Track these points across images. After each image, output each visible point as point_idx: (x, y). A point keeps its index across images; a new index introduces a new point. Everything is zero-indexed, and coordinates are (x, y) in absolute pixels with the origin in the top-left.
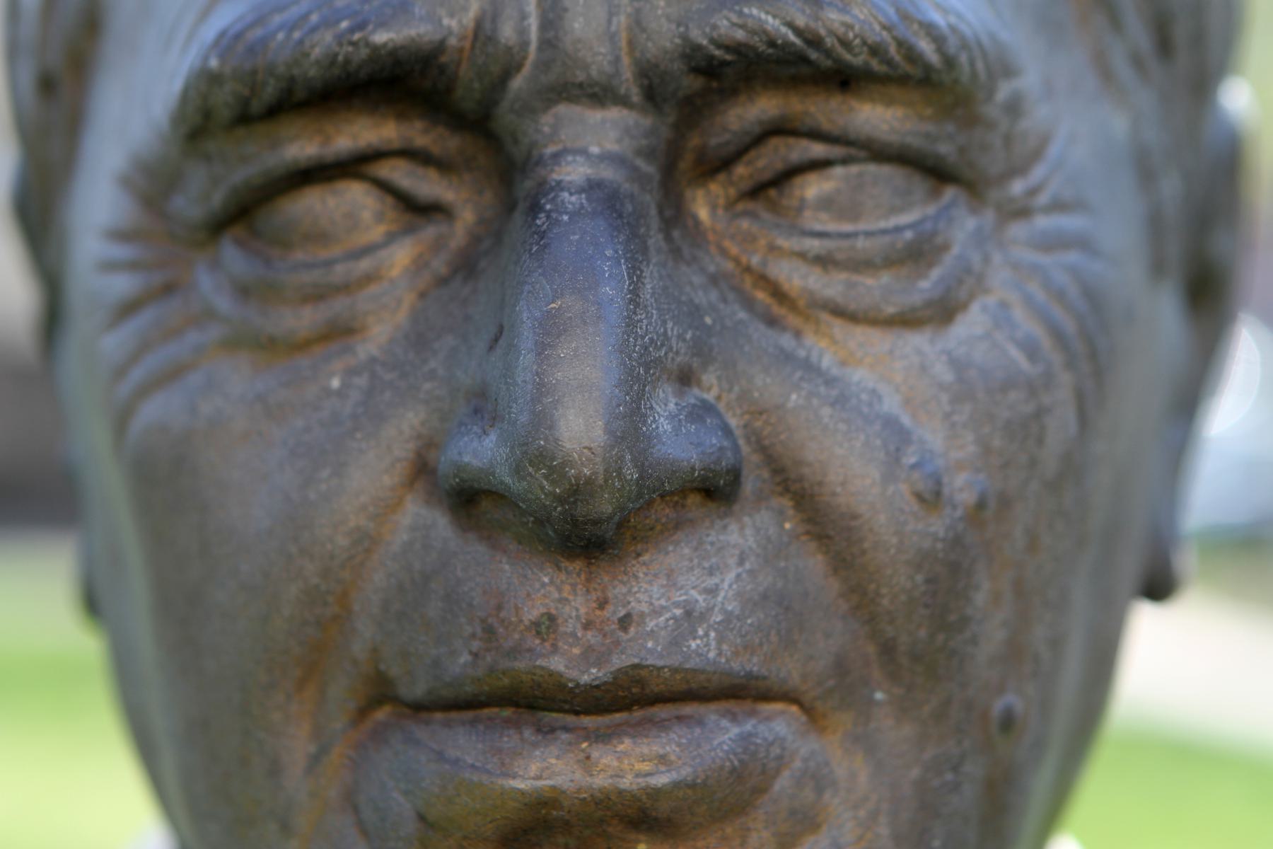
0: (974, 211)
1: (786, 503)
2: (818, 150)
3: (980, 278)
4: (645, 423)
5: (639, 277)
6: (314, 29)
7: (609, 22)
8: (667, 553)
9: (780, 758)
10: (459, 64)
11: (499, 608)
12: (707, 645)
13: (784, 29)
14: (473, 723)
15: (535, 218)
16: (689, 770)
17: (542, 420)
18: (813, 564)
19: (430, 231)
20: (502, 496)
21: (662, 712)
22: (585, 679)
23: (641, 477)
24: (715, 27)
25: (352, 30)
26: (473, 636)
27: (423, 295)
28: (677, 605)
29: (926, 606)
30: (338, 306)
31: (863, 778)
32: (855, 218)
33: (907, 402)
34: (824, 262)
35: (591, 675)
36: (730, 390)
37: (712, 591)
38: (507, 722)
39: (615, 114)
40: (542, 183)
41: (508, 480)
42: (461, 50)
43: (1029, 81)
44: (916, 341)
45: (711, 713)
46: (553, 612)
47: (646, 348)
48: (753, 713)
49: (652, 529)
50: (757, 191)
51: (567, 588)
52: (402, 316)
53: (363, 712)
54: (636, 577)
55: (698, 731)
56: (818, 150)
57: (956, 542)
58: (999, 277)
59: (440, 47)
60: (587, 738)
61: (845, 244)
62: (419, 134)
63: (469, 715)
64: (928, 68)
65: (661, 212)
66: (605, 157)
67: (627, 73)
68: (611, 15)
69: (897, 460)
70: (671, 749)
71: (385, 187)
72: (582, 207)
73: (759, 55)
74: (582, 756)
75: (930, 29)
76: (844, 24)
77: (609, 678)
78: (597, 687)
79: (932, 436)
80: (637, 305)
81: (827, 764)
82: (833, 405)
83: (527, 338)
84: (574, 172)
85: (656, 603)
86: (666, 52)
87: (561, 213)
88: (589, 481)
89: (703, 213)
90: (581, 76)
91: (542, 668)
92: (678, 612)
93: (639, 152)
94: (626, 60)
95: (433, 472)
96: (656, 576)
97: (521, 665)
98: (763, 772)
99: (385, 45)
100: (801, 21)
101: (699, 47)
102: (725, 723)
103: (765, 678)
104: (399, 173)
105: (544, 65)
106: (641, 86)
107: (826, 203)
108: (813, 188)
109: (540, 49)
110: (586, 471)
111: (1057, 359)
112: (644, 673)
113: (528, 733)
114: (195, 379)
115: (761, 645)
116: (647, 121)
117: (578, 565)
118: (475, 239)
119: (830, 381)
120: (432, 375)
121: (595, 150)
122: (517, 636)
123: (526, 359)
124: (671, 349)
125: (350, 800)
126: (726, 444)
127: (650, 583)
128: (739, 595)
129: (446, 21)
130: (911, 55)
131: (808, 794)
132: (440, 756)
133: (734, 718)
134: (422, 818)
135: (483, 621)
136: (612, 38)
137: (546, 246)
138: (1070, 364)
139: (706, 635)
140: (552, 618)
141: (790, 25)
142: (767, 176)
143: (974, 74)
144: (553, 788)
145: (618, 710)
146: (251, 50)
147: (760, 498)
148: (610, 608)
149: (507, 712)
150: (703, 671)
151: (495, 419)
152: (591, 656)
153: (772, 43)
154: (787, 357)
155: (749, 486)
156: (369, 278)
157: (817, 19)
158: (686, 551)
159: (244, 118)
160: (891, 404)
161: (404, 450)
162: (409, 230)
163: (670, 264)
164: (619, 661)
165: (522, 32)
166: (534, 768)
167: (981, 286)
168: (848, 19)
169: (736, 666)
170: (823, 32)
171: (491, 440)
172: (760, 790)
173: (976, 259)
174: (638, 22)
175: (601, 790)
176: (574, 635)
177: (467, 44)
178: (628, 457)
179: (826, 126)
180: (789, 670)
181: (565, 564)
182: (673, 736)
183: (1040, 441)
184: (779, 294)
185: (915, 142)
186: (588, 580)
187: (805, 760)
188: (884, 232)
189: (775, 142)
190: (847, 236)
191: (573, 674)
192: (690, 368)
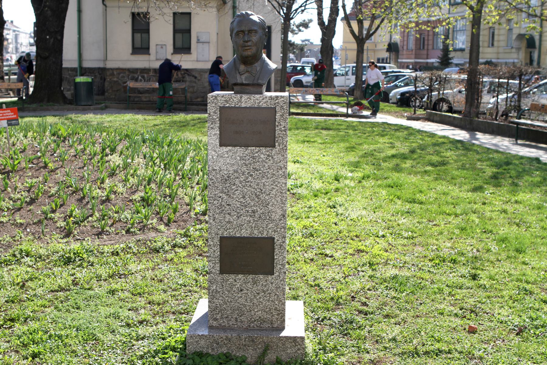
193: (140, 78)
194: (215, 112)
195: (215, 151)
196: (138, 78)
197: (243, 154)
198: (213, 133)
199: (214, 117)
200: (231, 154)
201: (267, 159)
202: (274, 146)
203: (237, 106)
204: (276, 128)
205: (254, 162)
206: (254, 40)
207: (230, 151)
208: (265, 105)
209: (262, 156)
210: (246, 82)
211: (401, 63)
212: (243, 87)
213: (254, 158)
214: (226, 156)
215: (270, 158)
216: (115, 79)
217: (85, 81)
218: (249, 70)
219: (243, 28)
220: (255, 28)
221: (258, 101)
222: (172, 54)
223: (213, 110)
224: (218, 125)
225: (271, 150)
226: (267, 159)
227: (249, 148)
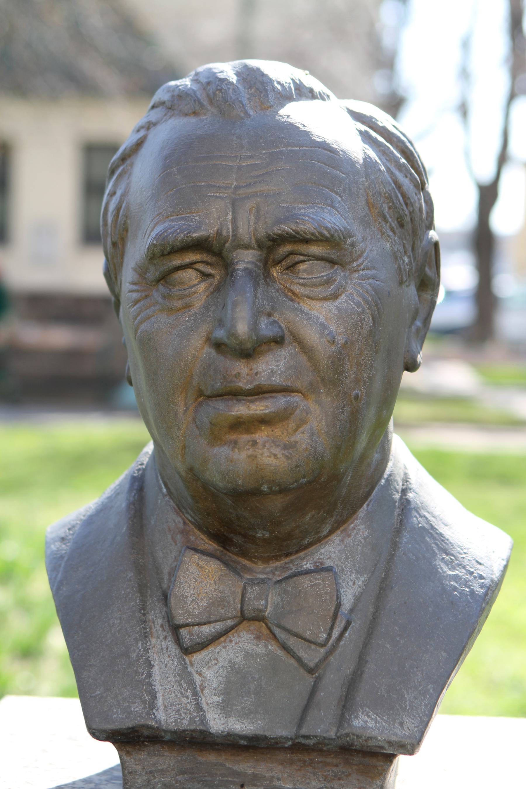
0: (343, 271)
1: (296, 344)
2: (302, 258)
3: (345, 287)
4: (258, 326)
5: (256, 291)
6: (178, 234)
7: (249, 230)
8: (266, 357)
9: (297, 406)
10: (213, 241)
11: (227, 371)
12: (277, 379)
13: (290, 230)
14: (222, 400)
15: (232, 278)
16: (273, 409)
17: (234, 326)
18: (304, 358)
19: (209, 281)
20: (226, 345)
21: (266, 395)
22: (247, 387)
23: (257, 339)
24: (274, 230)
25: (187, 234)
26: (221, 379)
27: (207, 297)
28: (269, 369)
29: (332, 368)
30: (187, 300)
31: (318, 411)
32: (312, 274)
33: (326, 319)
34: (304, 285)
35: (249, 387)
36: (281, 317)
37: (278, 366)
38: (230, 399)
39: (251, 251)
40: (234, 269)
41: (226, 340)
42: (214, 237)
43: (358, 237)
44: (328, 304)
45: (279, 395)
46: (239, 372)
47: (258, 308)
48: (290, 395)
49: (262, 351)
50: (288, 268)
51: (242, 366)
52: (202, 302)
53: (196, 399)
54: (259, 363)
55: (275, 400)
56: (302, 258)
57: (340, 352)
58: (350, 288)
59: (209, 237)
60: (248, 402)
61: (309, 280)
62: (205, 257)
63: (221, 398)
64: (327, 238)
65: (263, 274)
66: (249, 262)
67: (254, 242)
68: (249, 228)
69: (323, 333)
70: (269, 404)
71: (197, 270)
72: (243, 275)
73: (285, 236)
74: (247, 406)
75: (327, 228)
76: (305, 228)
77: (253, 387)
78: (250, 389)
79: (333, 327)
80: (256, 298)
81: (309, 407)
82: (307, 320)
83: (229, 307)
84: (241, 266)
85: (264, 369)
86: (262, 236)
87: (238, 276)
88: (244, 340)
89: (275, 274)
90: (242, 243)
91: (237, 385)
92: (269, 371)
93: (257, 261)
94: (253, 238)
95: (210, 340)
96: (264, 362)
97: (232, 385)
98: (292, 409)
99: (195, 237)
100: (294, 228)
101: (270, 235)
102: (282, 398)
103: (292, 387)
104: (200, 267)
105: (233, 241)
106: (257, 245)
107: (305, 271)
108: (302, 267)
109: (232, 236)
110: (244, 338)
111: (366, 307)
112: (261, 386)
113: (235, 401)
114: (153, 319)
115: (290, 379)
116: (259, 253)
117: (245, 360)
118: (220, 282)
119: (306, 314)
120: (210, 316)
121: (246, 260)
122: (231, 378)
123: (229, 312)
124: (265, 308)
125: (194, 420)
126: (279, 330)
127: (262, 364)
128: (285, 366)
129: (209, 231)
130: (322, 235)
131: (304, 414)
132: (214, 408)
133: (285, 397)
134: (211, 423)
135: (223, 375)
136: (249, 233)
137: (234, 284)
138: (370, 308)
139: (277, 376)
140: (239, 374)
141: (291, 229)
142: (290, 264)
143: (340, 238)
144: (241, 414)
145: (256, 395)
146: (164, 239)
147: (290, 343)
148: (253, 371)
149: (230, 397)
150: (276, 385)
151: (223, 326)
152: (249, 382)
153: (287, 234)
154: (296, 309)
155: (287, 341)
156: (194, 293)
157: (298, 227)
158: (271, 356)
159: (163, 255)
160: (322, 319)
161: (204, 335)
162: (204, 281)
163: (266, 287)
164: (256, 383)
165: (228, 232)
166: (236, 409)
167: (345, 289)
168: (305, 227)
169: (284, 384)
170: (299, 230)
171: (222, 332)
172: (291, 414)
173: (343, 283)
174: (255, 229)
175: (252, 414)
176: (244, 377)
177: (215, 236)
178: (254, 334)
179: (303, 252)
180: (298, 385)
181: (242, 360)
182: (269, 401)
183: (362, 328)
184: (294, 293)
185: (326, 255)
186: (248, 364)
187: (303, 407)
188: (319, 277)
189: (291, 256)
190: (310, 278)
191: (244, 386)
192: (271, 313)
212: (211, 758)
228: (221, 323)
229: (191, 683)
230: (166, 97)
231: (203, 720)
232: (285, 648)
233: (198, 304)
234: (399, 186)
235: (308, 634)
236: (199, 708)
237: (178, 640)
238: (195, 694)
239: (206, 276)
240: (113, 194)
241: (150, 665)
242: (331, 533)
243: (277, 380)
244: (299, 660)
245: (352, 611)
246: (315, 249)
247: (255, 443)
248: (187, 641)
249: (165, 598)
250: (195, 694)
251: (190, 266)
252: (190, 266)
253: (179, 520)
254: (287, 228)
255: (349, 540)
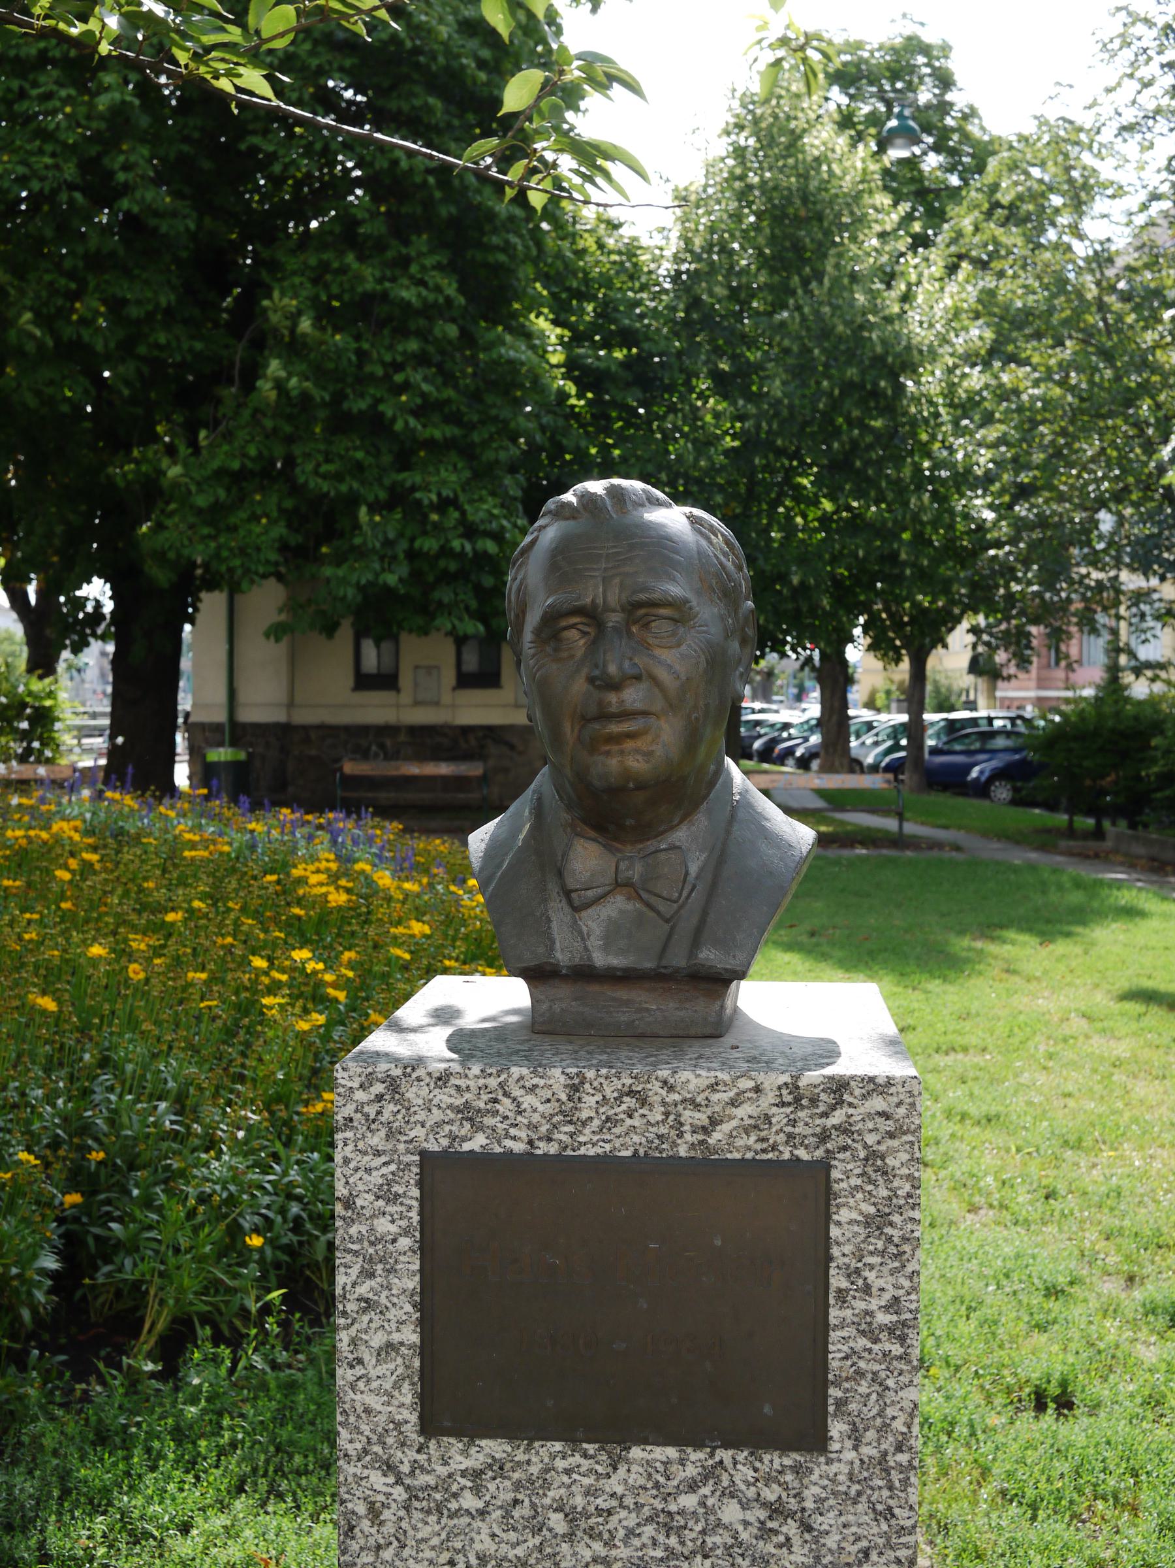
43: (694, 603)
62: (584, 620)
193: (374, 748)
194: (386, 1193)
195: (389, 1467)
196: (369, 749)
197: (589, 1492)
198: (378, 1340)
199: (384, 1226)
200: (500, 1490)
201: (766, 1533)
202: (817, 1442)
203: (543, 1148)
204: (835, 1315)
205: (671, 1553)
206: (663, 674)
207: (499, 1468)
208: (746, 1147)
209: (731, 1512)
210: (616, 961)
211: (1003, 699)
212: (596, 988)
213: (668, 1523)
214: (470, 1502)
215: (791, 1528)
216: (313, 752)
217: (229, 758)
218: (636, 872)
219: (590, 593)
220: (675, 590)
221: (701, 1118)
222: (454, 689)
223: (376, 1178)
224: (413, 1283)
225: (797, 1469)
226: (766, 1533)
227: (636, 1452)
228: (596, 666)
229: (580, 933)
230: (553, 507)
231: (590, 958)
232: (648, 905)
233: (579, 653)
234: (723, 567)
235: (665, 894)
236: (586, 949)
237: (570, 902)
238: (583, 939)
239: (585, 633)
240: (514, 579)
241: (549, 920)
242: (681, 822)
243: (638, 706)
244: (658, 913)
245: (696, 878)
246: (663, 611)
247: (622, 752)
248: (577, 903)
249: (560, 874)
250: (583, 939)
251: (573, 626)
252: (573, 626)
253: (568, 817)
254: (643, 597)
255: (694, 828)
